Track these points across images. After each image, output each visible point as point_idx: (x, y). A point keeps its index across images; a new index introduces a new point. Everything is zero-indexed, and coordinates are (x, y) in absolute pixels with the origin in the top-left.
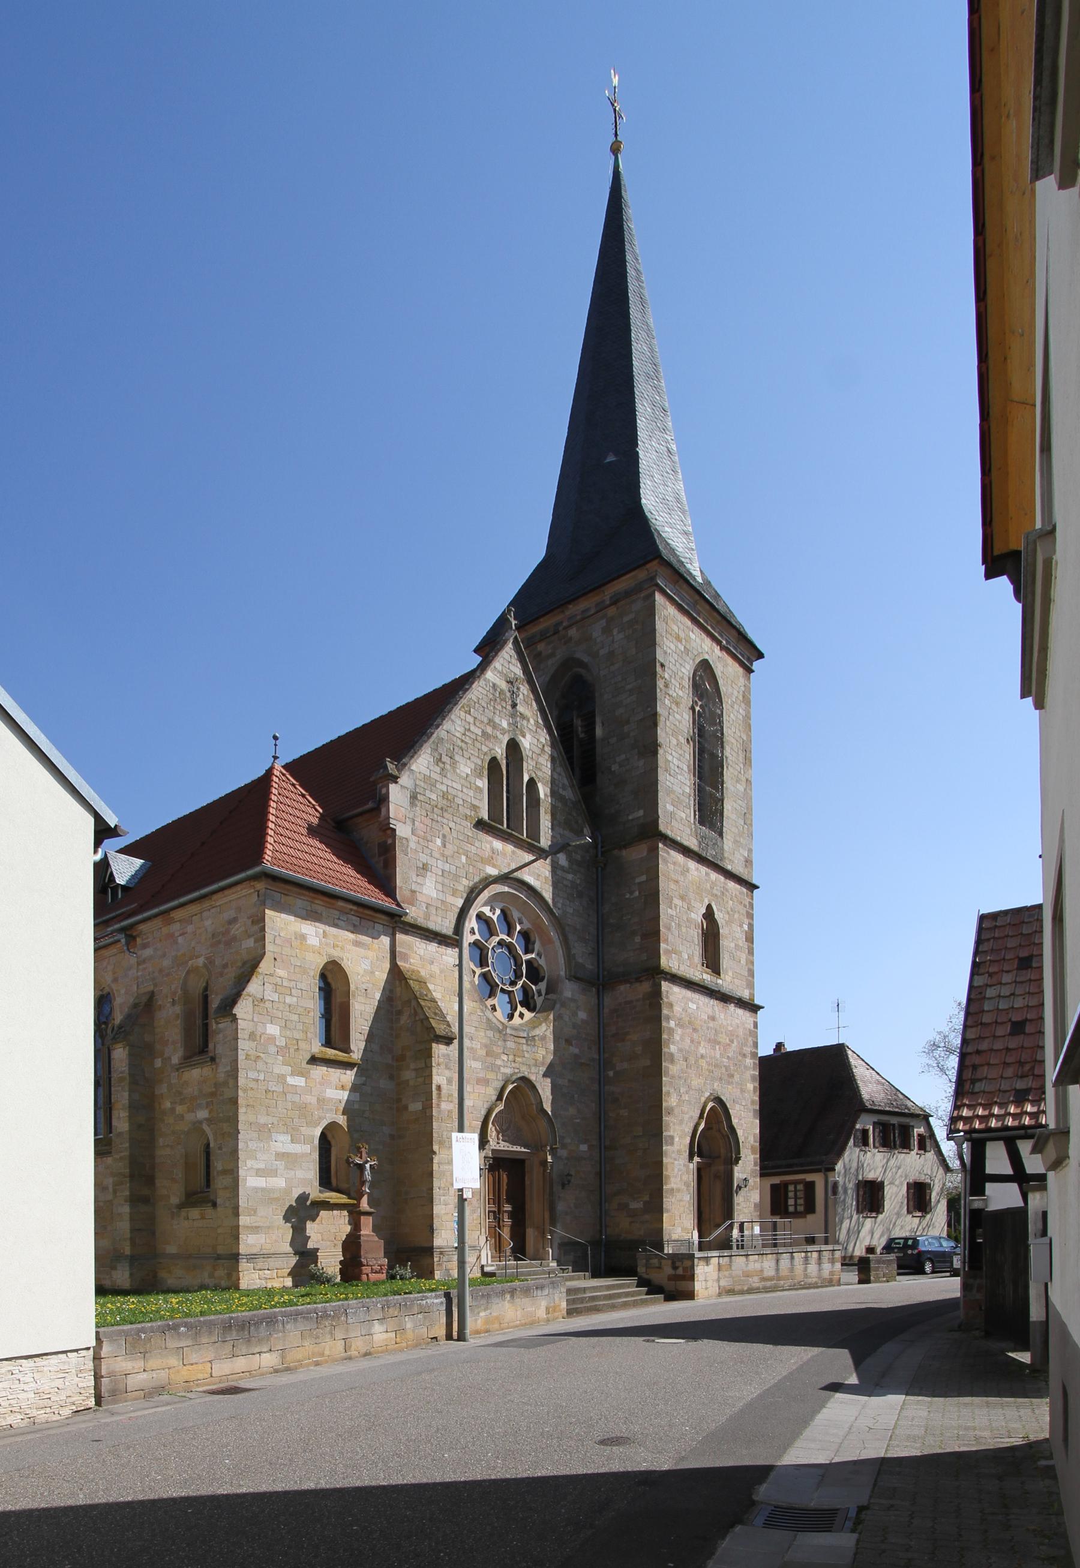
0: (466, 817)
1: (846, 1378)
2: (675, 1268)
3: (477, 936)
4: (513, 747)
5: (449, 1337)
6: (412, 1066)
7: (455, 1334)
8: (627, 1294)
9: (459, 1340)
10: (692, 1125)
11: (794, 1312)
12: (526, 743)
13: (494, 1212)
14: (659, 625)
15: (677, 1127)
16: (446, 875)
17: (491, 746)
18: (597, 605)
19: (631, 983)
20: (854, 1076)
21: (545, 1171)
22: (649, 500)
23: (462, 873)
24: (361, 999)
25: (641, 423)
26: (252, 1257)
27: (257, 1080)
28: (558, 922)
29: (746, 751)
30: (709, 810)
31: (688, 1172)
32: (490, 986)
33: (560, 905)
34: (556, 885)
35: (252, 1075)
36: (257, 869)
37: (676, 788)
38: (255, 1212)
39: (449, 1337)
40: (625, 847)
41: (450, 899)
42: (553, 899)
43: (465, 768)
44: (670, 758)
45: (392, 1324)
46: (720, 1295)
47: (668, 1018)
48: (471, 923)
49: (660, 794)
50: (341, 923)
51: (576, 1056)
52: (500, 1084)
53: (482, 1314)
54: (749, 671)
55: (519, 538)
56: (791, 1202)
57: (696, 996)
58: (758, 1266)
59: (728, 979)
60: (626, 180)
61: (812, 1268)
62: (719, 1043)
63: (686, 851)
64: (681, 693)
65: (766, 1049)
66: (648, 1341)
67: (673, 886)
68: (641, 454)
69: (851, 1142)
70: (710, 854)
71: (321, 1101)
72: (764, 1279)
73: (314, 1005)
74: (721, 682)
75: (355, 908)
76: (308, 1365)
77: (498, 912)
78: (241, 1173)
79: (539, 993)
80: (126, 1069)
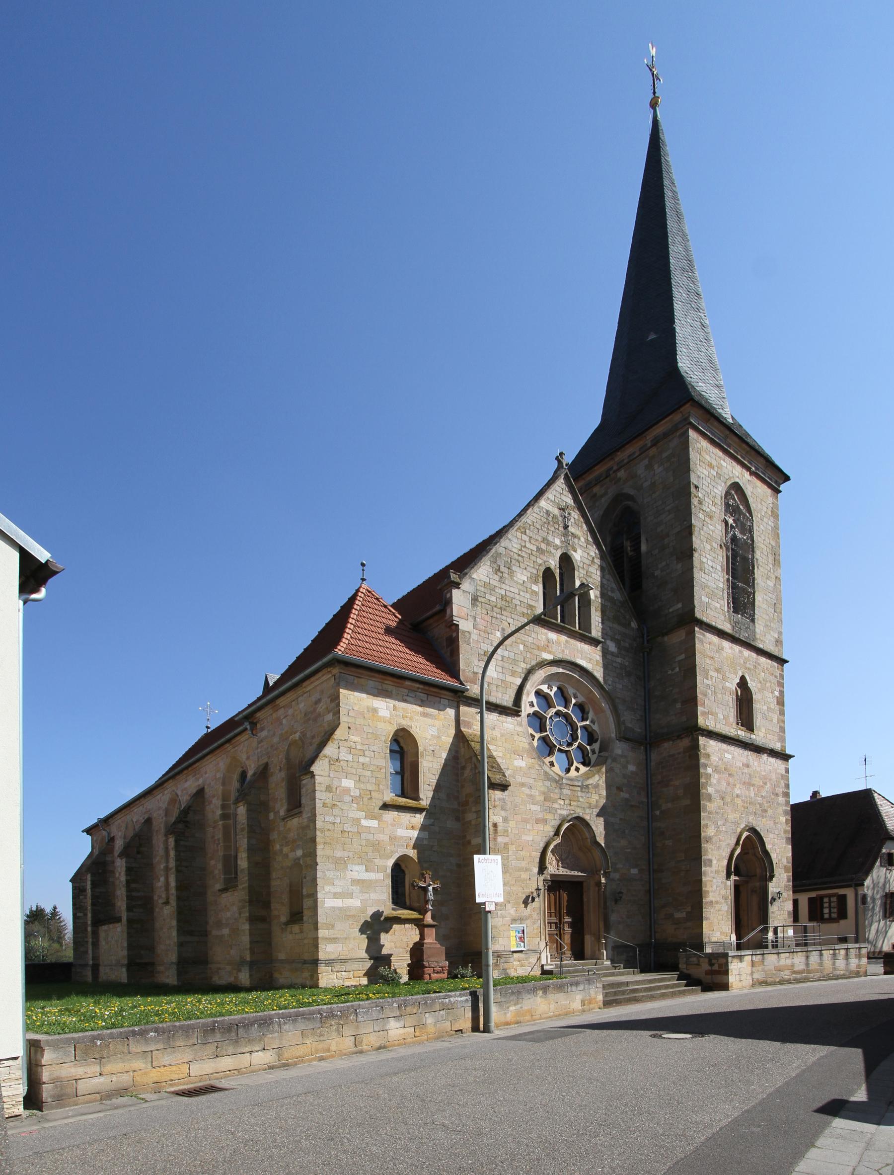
1: (852, 1092)
2: (711, 965)
3: (536, 708)
4: (566, 561)
5: (475, 1028)
6: (474, 809)
7: (481, 1026)
8: (667, 987)
9: (484, 1032)
11: (816, 1003)
12: (577, 556)
13: (556, 923)
14: (693, 455)
15: (715, 852)
16: (505, 659)
17: (545, 558)
18: (640, 449)
19: (673, 741)
20: (880, 813)
21: (599, 890)
22: (684, 363)
23: (520, 658)
24: (430, 758)
25: (678, 306)
26: (330, 962)
27: (334, 823)
28: (609, 696)
29: (776, 555)
30: (742, 599)
31: (725, 887)
32: (547, 747)
33: (610, 683)
35: (329, 819)
36: (329, 657)
37: (712, 584)
38: (333, 926)
39: (475, 1028)
40: (666, 634)
41: (509, 679)
42: (604, 678)
43: (522, 576)
44: (705, 560)
45: (410, 1021)
46: (753, 985)
47: (705, 766)
48: (529, 697)
49: (696, 589)
50: (409, 699)
51: (627, 800)
52: (557, 823)
53: (512, 1008)
54: (777, 491)
55: (579, 413)
56: (826, 911)
57: (732, 748)
58: (789, 962)
59: (761, 734)
60: (666, 136)
61: (841, 963)
62: (753, 785)
63: (721, 634)
64: (714, 509)
65: (800, 795)
66: (655, 1036)
67: (708, 661)
68: (678, 329)
69: (878, 863)
70: (743, 636)
71: (393, 839)
72: (795, 972)
73: (386, 766)
74: (750, 500)
75: (421, 686)
76: (310, 1061)
77: (555, 689)
78: (319, 895)
79: (593, 752)
80: (245, 821)
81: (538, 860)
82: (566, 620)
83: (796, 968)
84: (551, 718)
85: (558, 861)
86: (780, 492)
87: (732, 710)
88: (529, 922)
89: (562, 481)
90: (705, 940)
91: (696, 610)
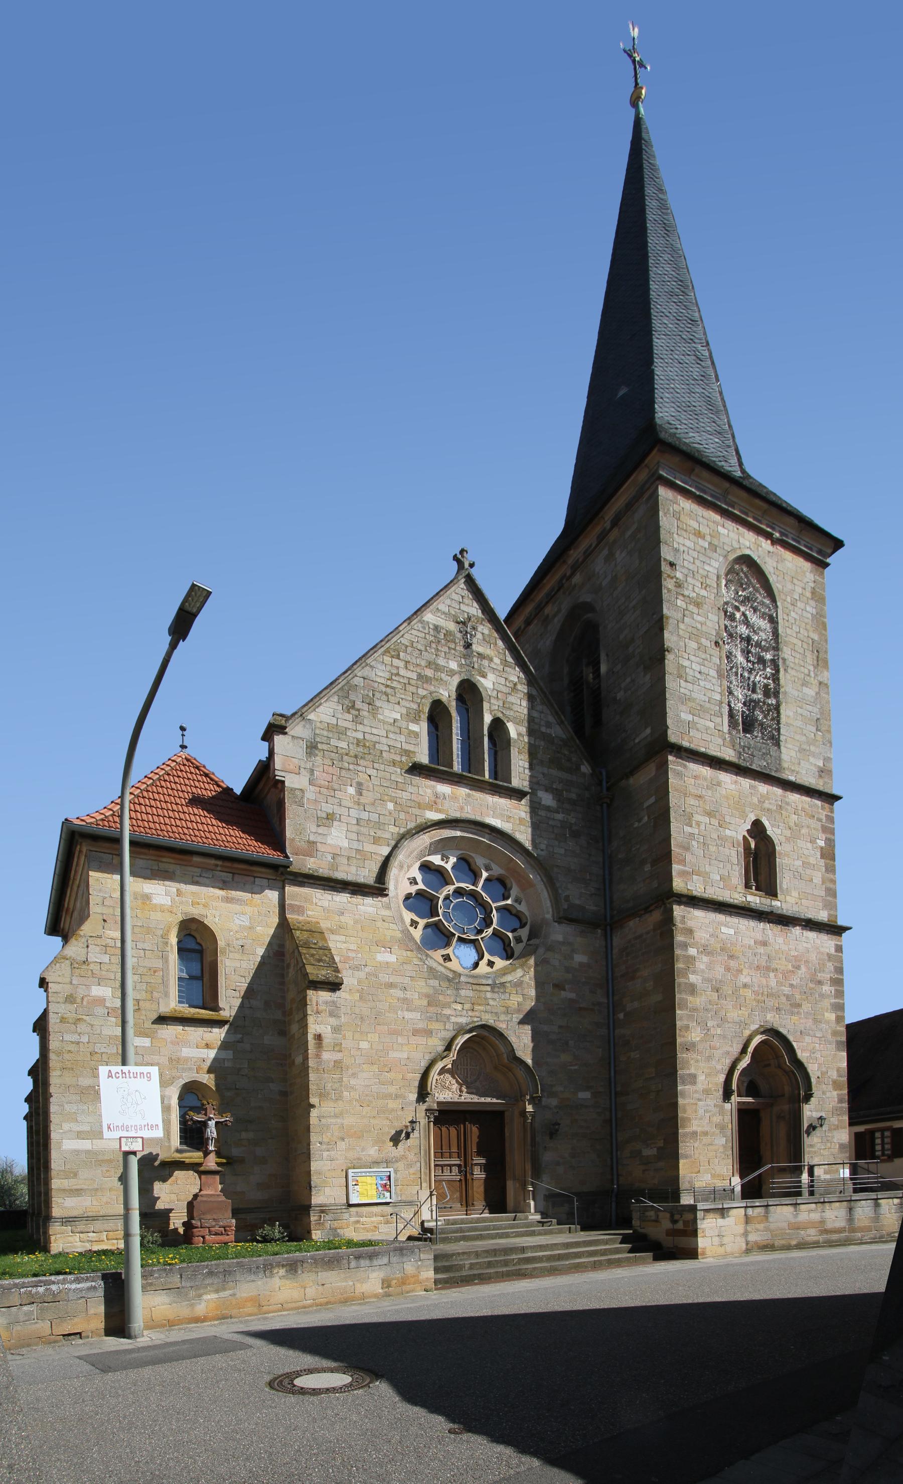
0: (394, 763)
2: (674, 1222)
3: (421, 886)
4: (469, 693)
10: (728, 1062)
12: (487, 683)
13: (459, 1166)
14: (665, 521)
16: (362, 823)
17: (432, 688)
21: (525, 1121)
25: (659, 343)
26: (67, 1221)
27: (78, 1043)
30: (757, 718)
32: (440, 936)
33: (543, 847)
34: (536, 826)
37: (699, 696)
38: (75, 1175)
40: (632, 773)
41: (369, 847)
43: (391, 713)
44: (686, 663)
46: (748, 1251)
47: (685, 946)
50: (201, 880)
57: (734, 920)
58: (815, 1216)
60: (654, 134)
64: (703, 593)
72: (826, 1231)
74: (772, 579)
75: (219, 863)
77: (453, 860)
81: (417, 1084)
82: (472, 770)
83: (829, 1225)
84: (447, 898)
85: (461, 1085)
86: (827, 565)
87: (736, 868)
88: (400, 1165)
89: (463, 586)
90: (684, 1184)
91: (669, 732)
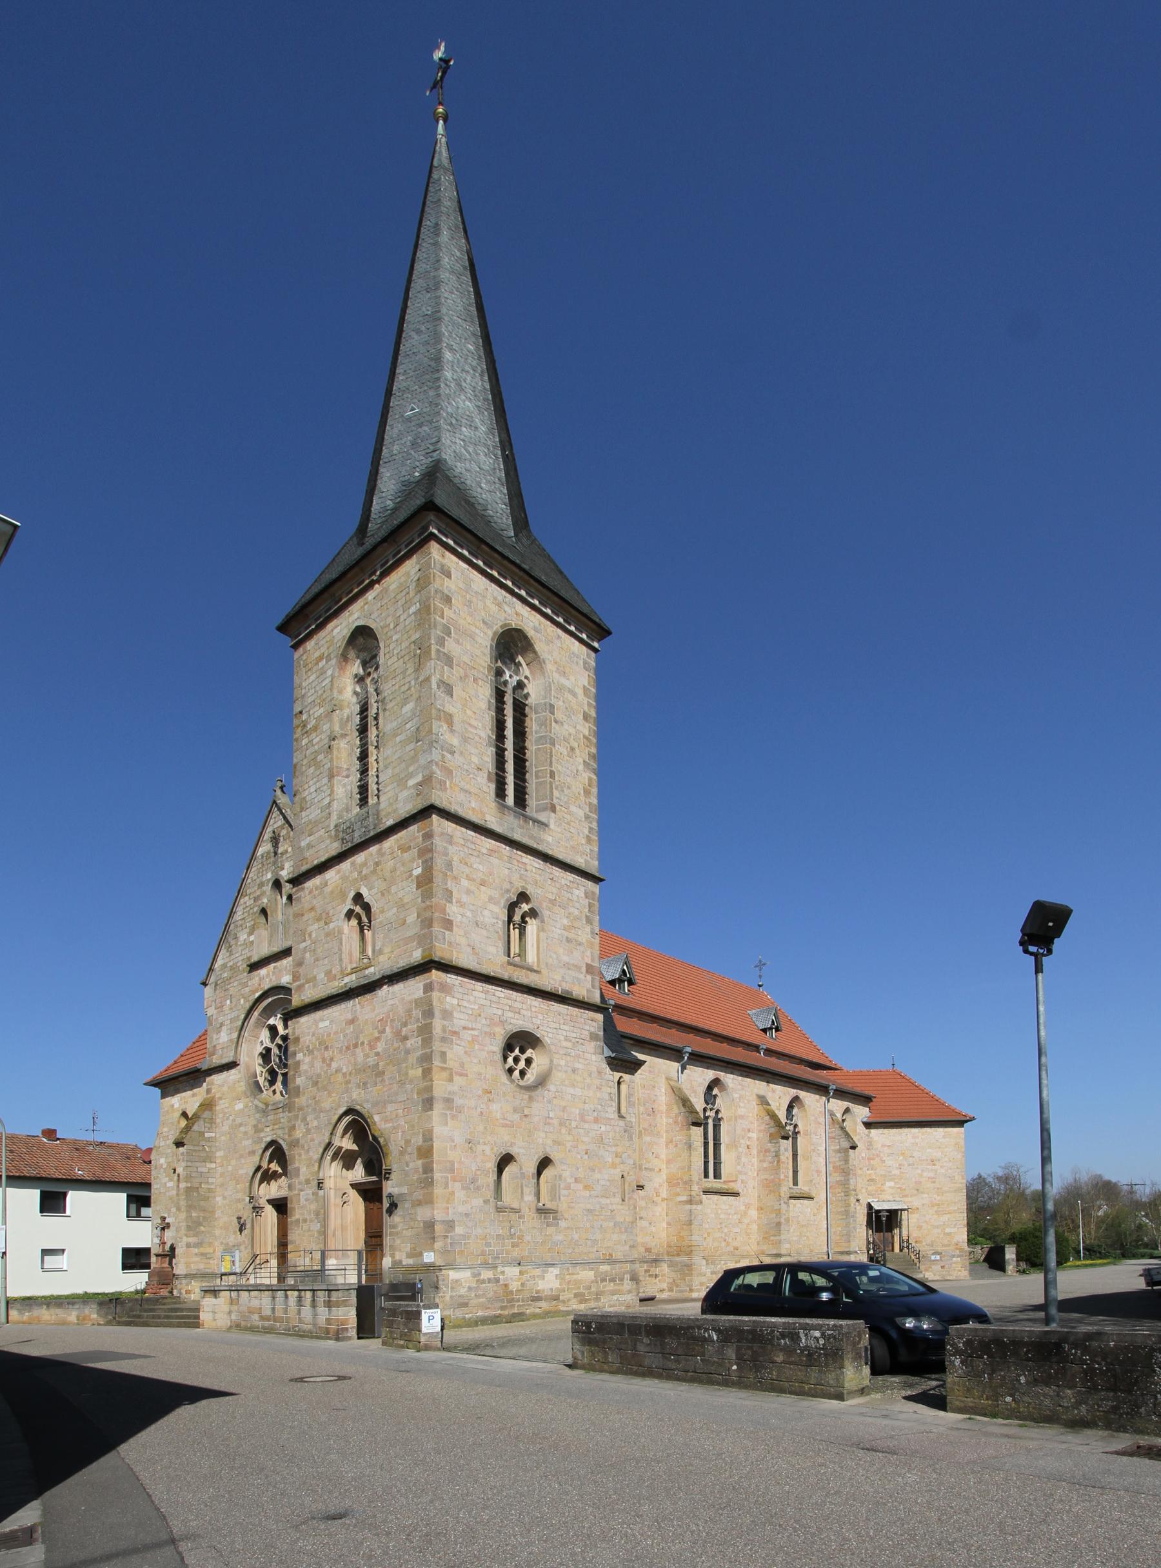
72: (262, 1318)
